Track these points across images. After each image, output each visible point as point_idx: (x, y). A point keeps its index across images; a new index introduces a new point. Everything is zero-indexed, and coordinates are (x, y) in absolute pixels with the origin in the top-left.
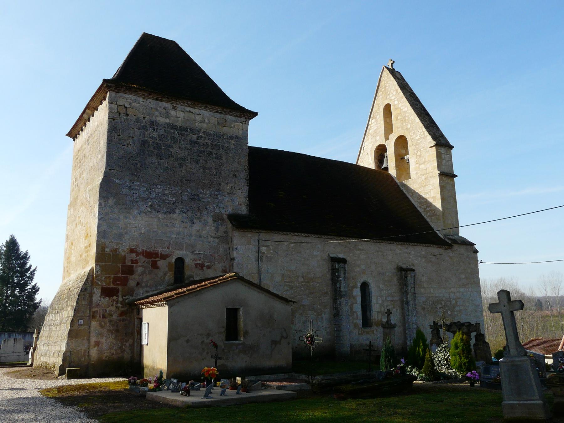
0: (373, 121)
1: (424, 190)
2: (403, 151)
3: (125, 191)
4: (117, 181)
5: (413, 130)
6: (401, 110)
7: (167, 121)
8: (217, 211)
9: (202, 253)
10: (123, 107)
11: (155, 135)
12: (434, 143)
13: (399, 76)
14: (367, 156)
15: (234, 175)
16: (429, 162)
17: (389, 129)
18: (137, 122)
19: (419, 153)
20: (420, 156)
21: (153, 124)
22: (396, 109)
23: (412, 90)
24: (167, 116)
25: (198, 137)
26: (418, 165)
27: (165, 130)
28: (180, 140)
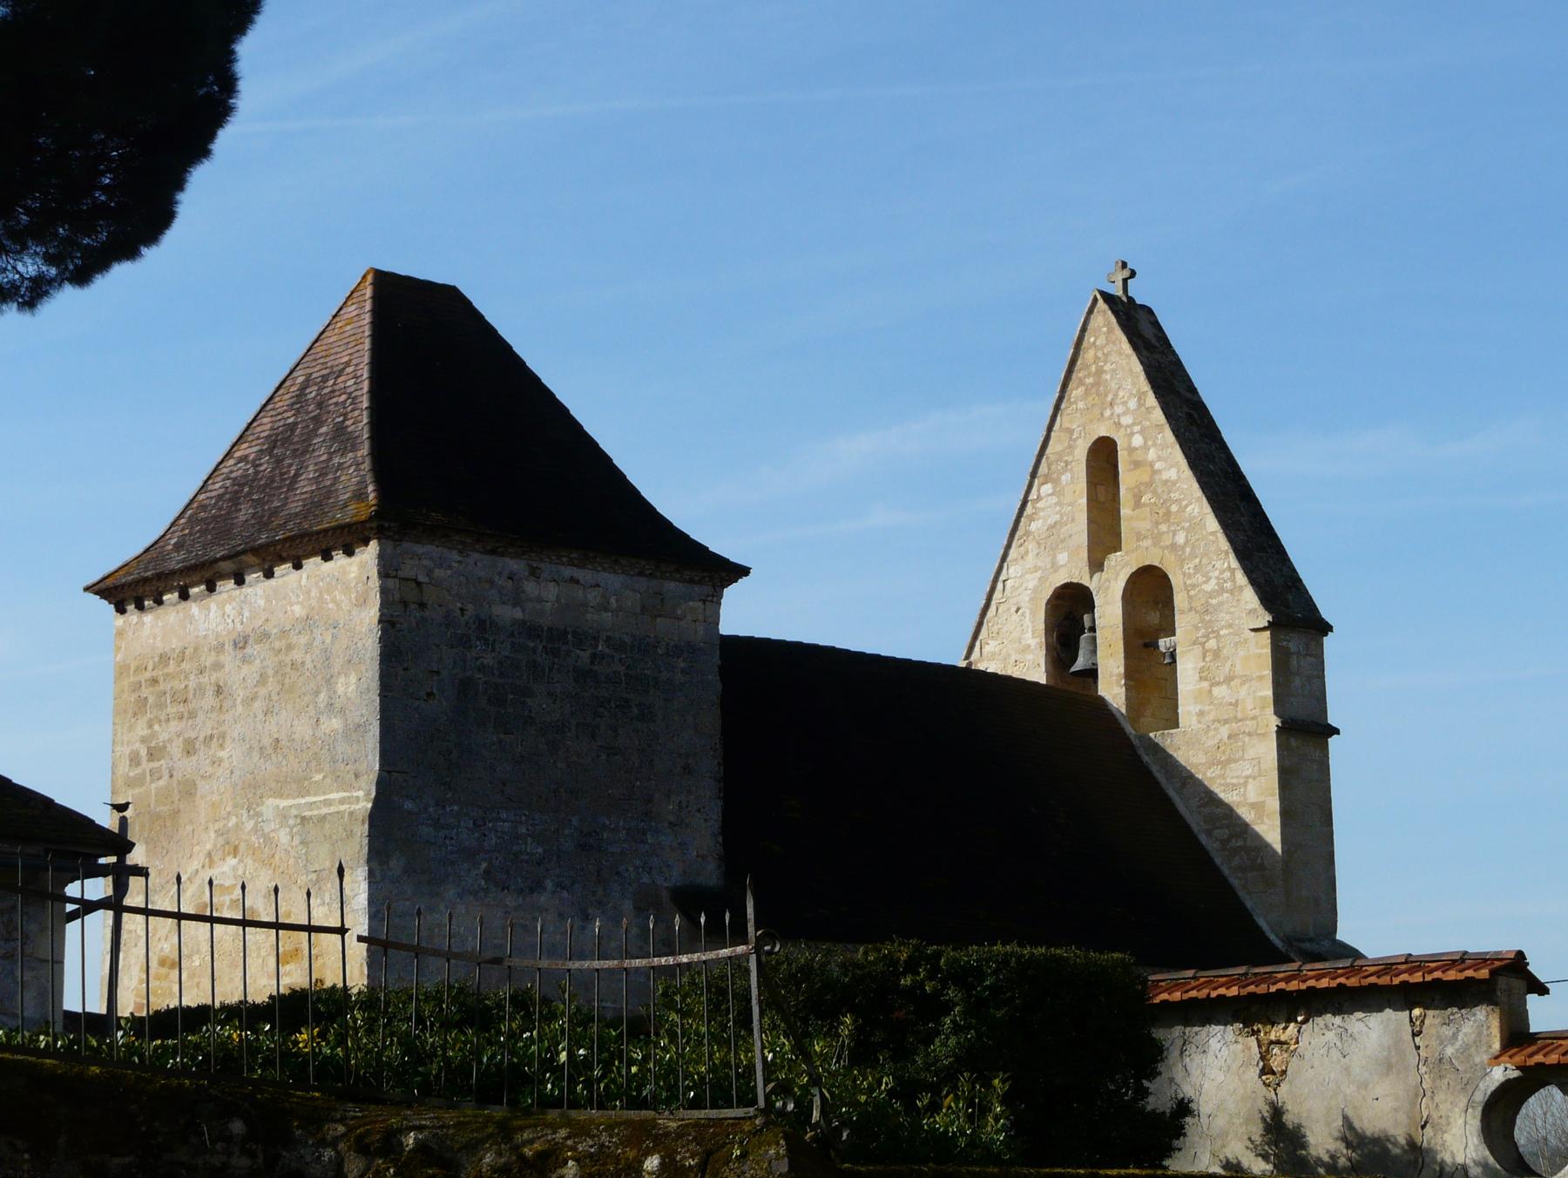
0: (1047, 488)
1: (1223, 776)
2: (1154, 618)
3: (426, 831)
4: (408, 805)
5: (1193, 556)
6: (1155, 472)
7: (518, 614)
8: (646, 879)
9: (609, 1004)
10: (413, 585)
11: (489, 660)
12: (1264, 618)
13: (1148, 332)
14: (1015, 617)
15: (686, 768)
16: (1246, 679)
17: (1105, 533)
18: (447, 626)
19: (1212, 644)
20: (1217, 654)
21: (484, 626)
22: (1137, 464)
23: (1194, 390)
24: (517, 599)
25: (594, 656)
26: (1205, 684)
27: (513, 644)
28: (551, 669)
